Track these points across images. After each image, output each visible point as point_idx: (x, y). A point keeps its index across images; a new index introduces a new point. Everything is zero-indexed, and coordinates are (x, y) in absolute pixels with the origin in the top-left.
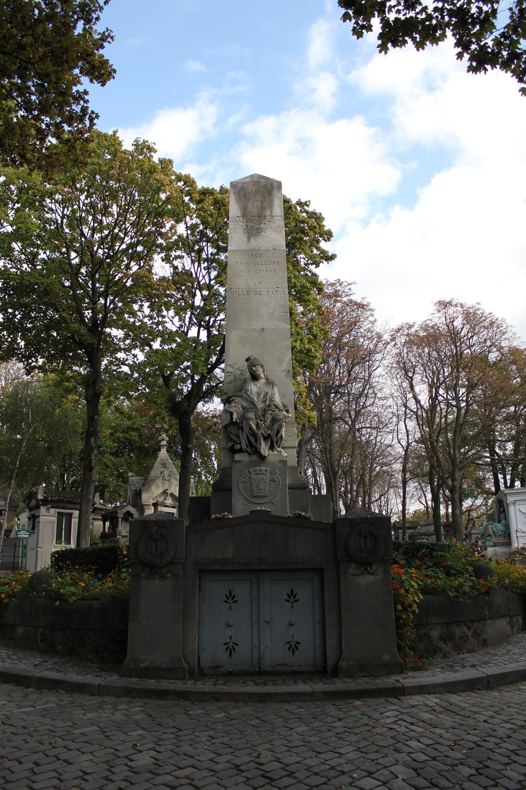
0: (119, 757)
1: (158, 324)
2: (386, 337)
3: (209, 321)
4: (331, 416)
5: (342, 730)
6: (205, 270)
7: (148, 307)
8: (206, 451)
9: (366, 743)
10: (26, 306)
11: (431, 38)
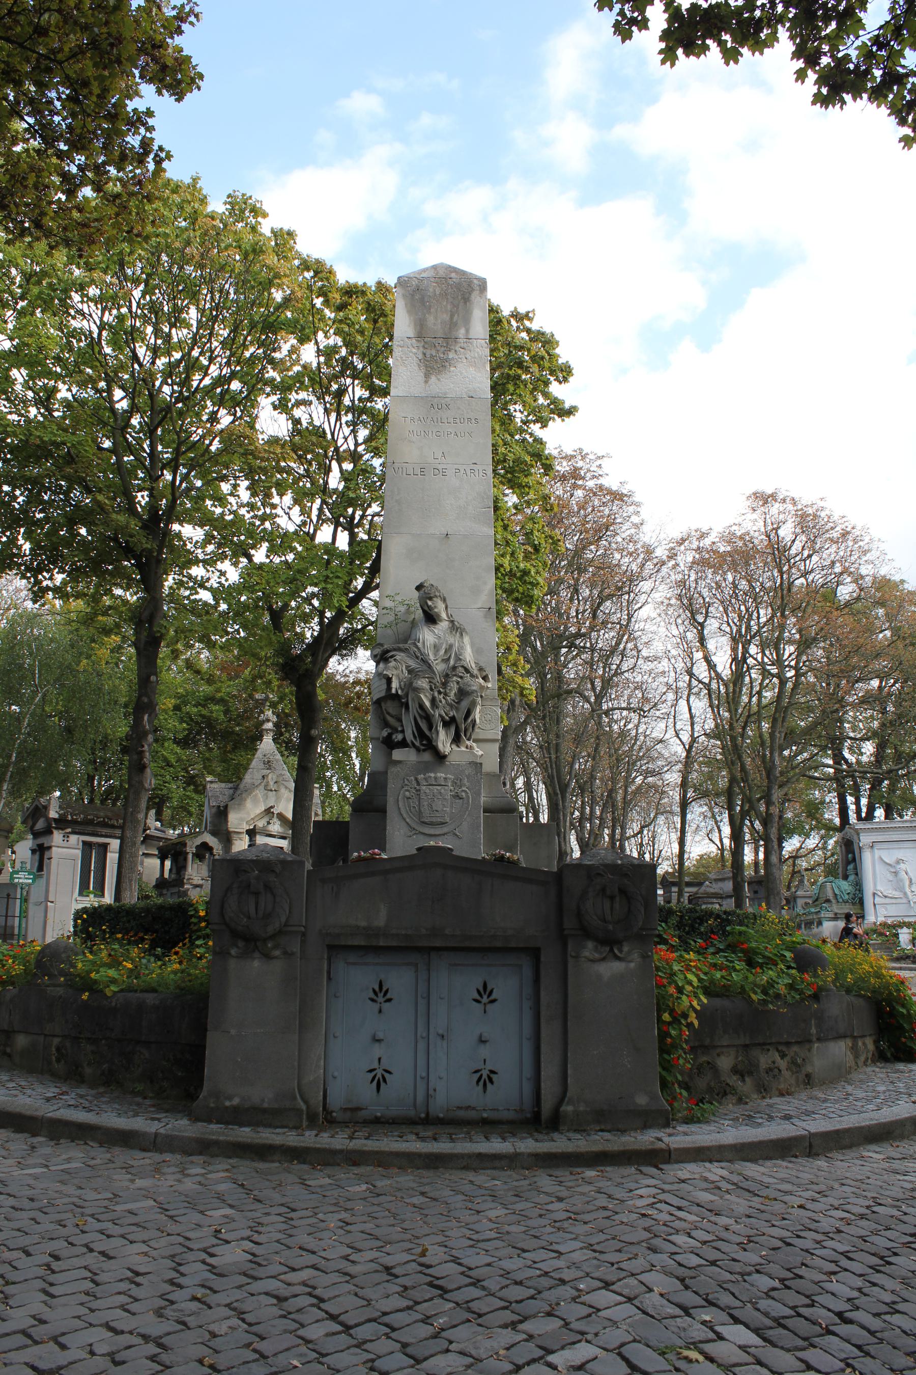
0: (192, 1250)
1: (263, 519)
2: (661, 552)
3: (353, 517)
4: (559, 687)
5: (565, 1215)
6: (348, 426)
7: (247, 488)
8: (342, 742)
9: (602, 1237)
10: (35, 481)
11: (751, 42)
